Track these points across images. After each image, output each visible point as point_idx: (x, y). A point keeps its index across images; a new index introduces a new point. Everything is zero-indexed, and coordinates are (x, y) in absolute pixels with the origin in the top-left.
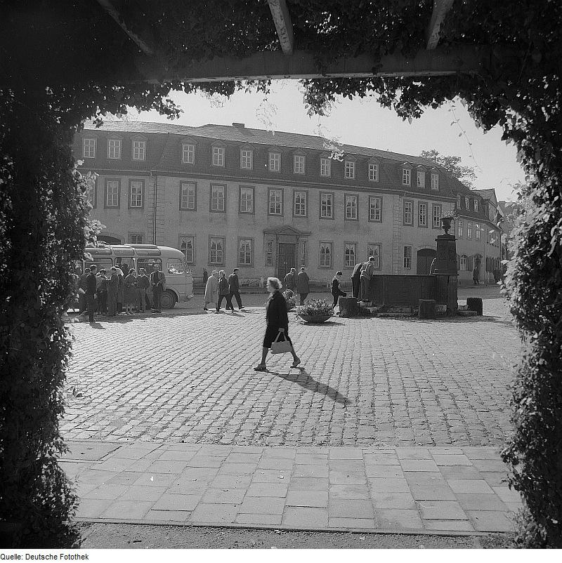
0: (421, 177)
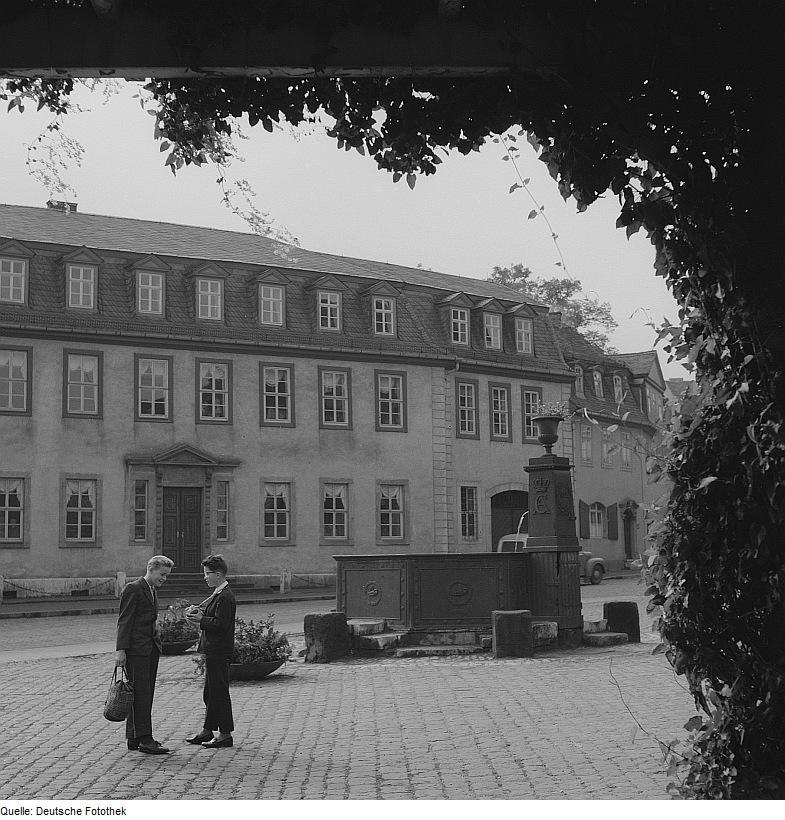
0: (493, 325)
